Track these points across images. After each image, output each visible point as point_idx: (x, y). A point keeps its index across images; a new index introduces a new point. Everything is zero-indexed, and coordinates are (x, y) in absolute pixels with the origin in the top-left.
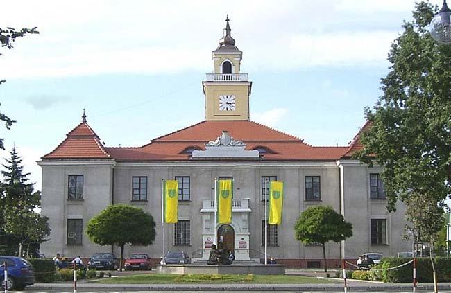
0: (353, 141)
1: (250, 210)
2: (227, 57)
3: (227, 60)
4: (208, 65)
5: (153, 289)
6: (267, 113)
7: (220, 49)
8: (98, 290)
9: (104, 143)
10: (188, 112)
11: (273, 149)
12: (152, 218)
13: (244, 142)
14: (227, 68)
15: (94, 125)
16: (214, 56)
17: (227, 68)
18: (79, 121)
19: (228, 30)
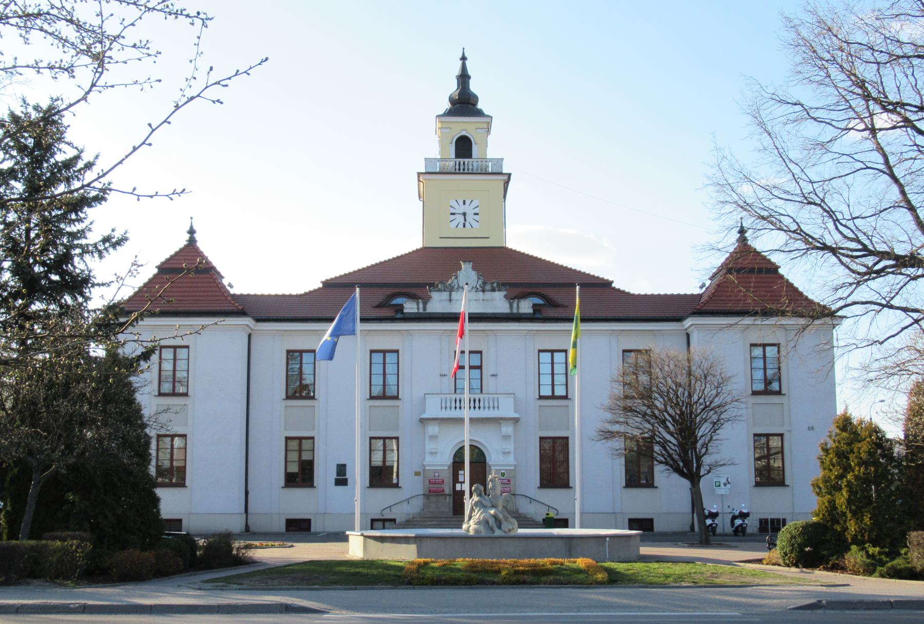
0: (708, 283)
1: (516, 415)
2: (464, 126)
3: (464, 133)
4: (431, 144)
5: (85, 609)
6: (534, 229)
7: (449, 113)
8: (399, 543)
9: (231, 286)
10: (392, 232)
11: (547, 294)
12: (876, 430)
13: (504, 285)
14: (464, 147)
15: (213, 250)
16: (439, 125)
17: (464, 147)
18: (181, 241)
19: (464, 78)
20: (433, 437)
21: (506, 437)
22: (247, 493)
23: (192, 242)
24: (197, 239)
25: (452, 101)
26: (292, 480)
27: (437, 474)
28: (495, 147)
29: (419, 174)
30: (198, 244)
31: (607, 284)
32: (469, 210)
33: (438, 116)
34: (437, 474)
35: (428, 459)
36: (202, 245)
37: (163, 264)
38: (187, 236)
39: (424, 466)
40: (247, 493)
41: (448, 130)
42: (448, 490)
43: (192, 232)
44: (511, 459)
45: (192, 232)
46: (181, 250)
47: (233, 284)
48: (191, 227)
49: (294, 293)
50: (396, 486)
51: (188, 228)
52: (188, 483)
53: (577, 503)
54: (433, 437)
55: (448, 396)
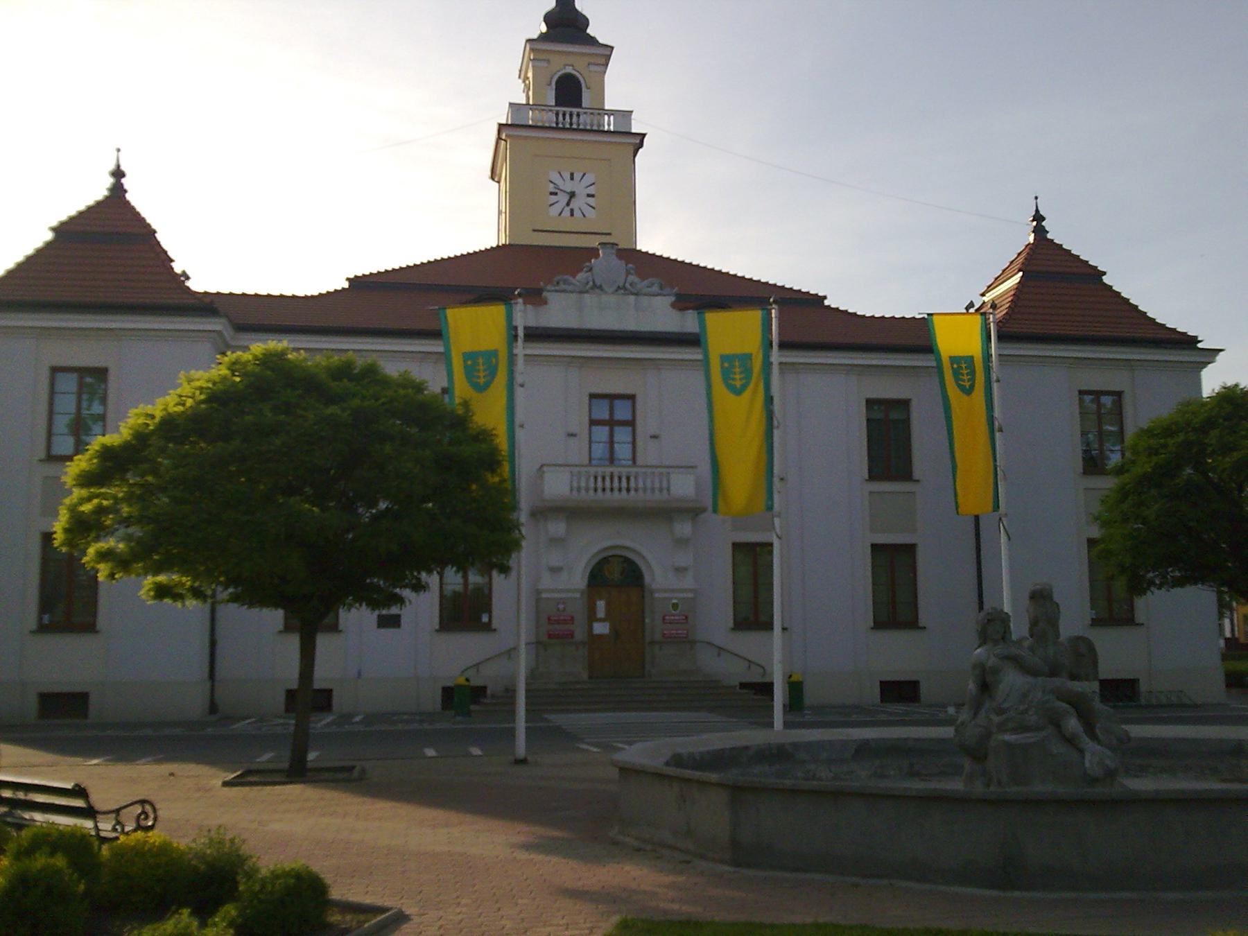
2: (568, 59)
3: (569, 70)
17: (569, 91)
18: (99, 190)
20: (556, 541)
21: (682, 542)
22: (213, 644)
23: (118, 191)
24: (126, 187)
25: (548, 18)
26: (742, 624)
27: (561, 607)
28: (619, 89)
29: (500, 125)
30: (128, 196)
31: (819, 300)
32: (580, 188)
33: (529, 41)
34: (561, 607)
35: (547, 581)
36: (134, 197)
37: (63, 224)
38: (110, 181)
39: (538, 592)
40: (213, 644)
41: (545, 64)
42: (580, 635)
43: (118, 174)
44: (688, 582)
45: (118, 174)
46: (99, 204)
47: (188, 273)
48: (118, 166)
49: (301, 294)
50: (488, 628)
51: (112, 167)
52: (102, 621)
53: (777, 656)
54: (556, 541)
55: (600, 470)
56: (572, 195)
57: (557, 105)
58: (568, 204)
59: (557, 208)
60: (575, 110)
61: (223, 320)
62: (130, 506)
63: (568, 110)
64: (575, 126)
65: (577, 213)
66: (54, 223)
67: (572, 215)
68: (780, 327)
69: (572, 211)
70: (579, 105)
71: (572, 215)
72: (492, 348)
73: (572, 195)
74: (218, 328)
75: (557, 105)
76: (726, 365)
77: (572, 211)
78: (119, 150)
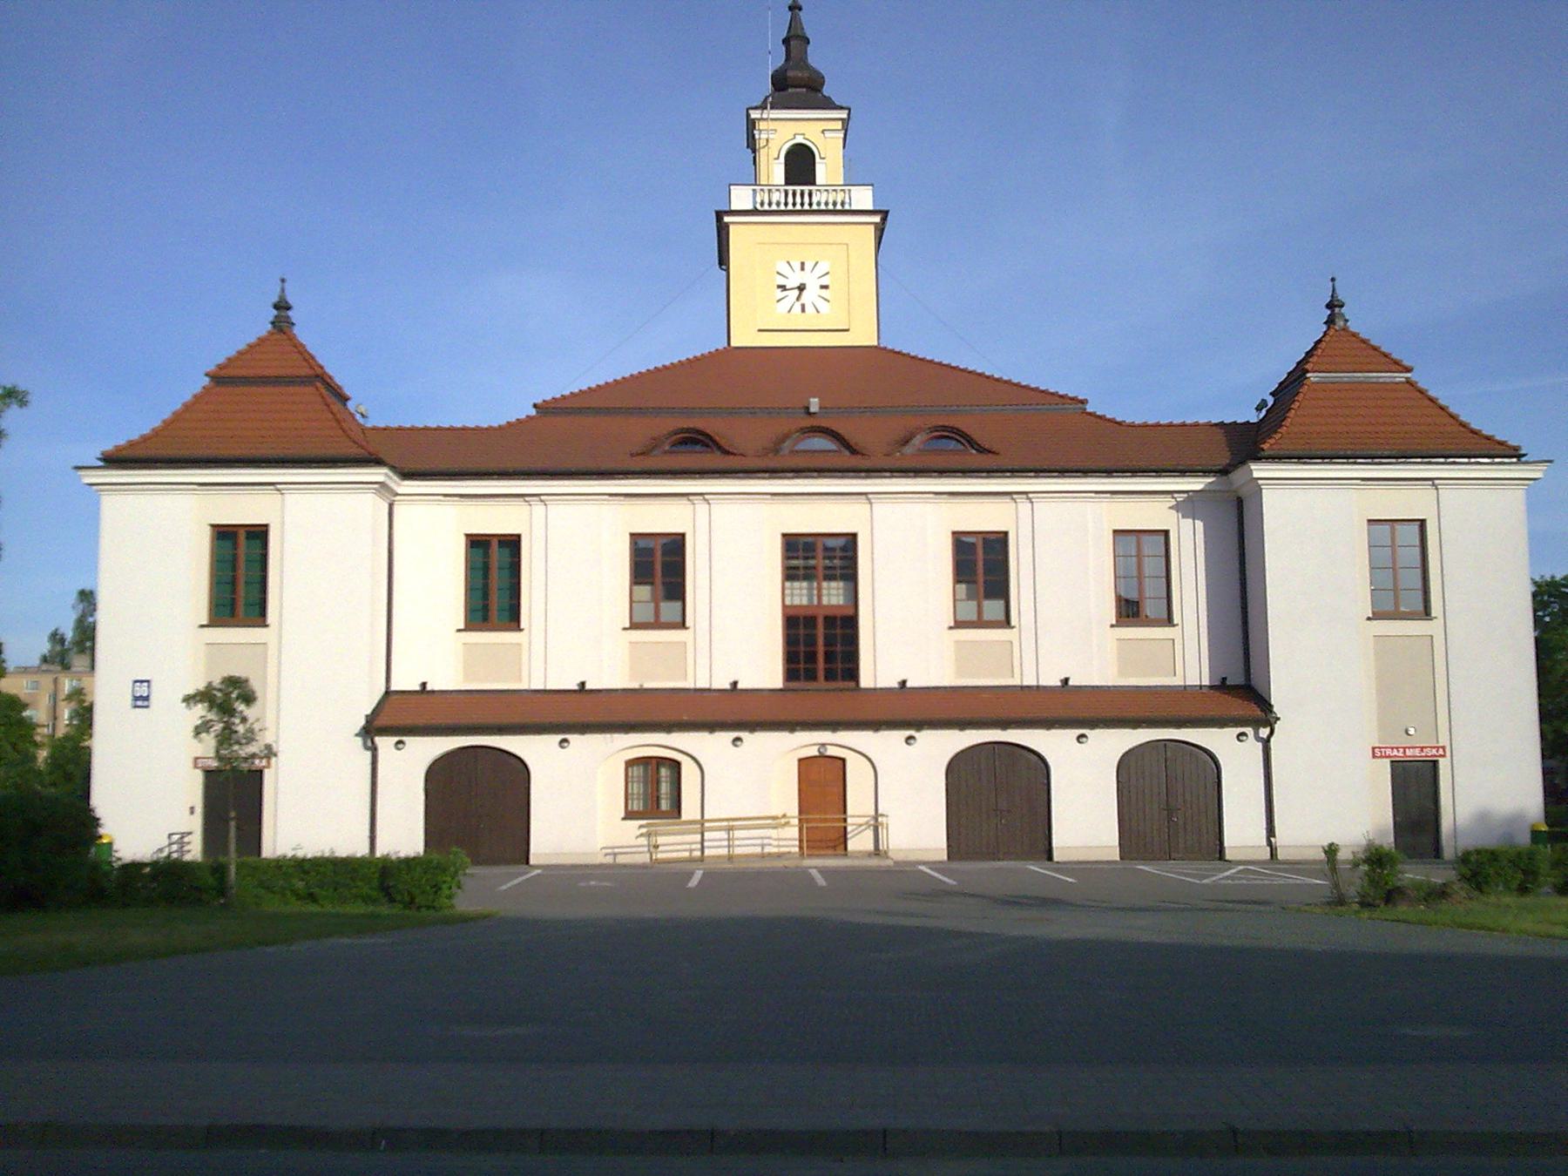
3: (800, 140)
51: (275, 299)
56: (801, 288)
57: (787, 183)
58: (798, 299)
59: (786, 304)
60: (806, 188)
61: (385, 470)
62: (46, 759)
63: (798, 188)
64: (806, 207)
65: (809, 308)
66: (211, 368)
67: (803, 310)
68: (228, 832)
69: (803, 307)
70: (814, 183)
71: (803, 310)
72: (1359, 539)
73: (801, 288)
74: (381, 479)
75: (787, 183)
76: (88, 644)
77: (803, 307)
78: (283, 281)
